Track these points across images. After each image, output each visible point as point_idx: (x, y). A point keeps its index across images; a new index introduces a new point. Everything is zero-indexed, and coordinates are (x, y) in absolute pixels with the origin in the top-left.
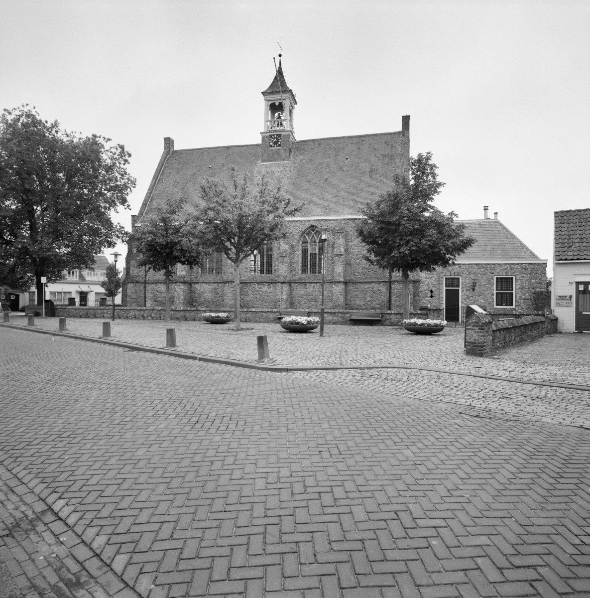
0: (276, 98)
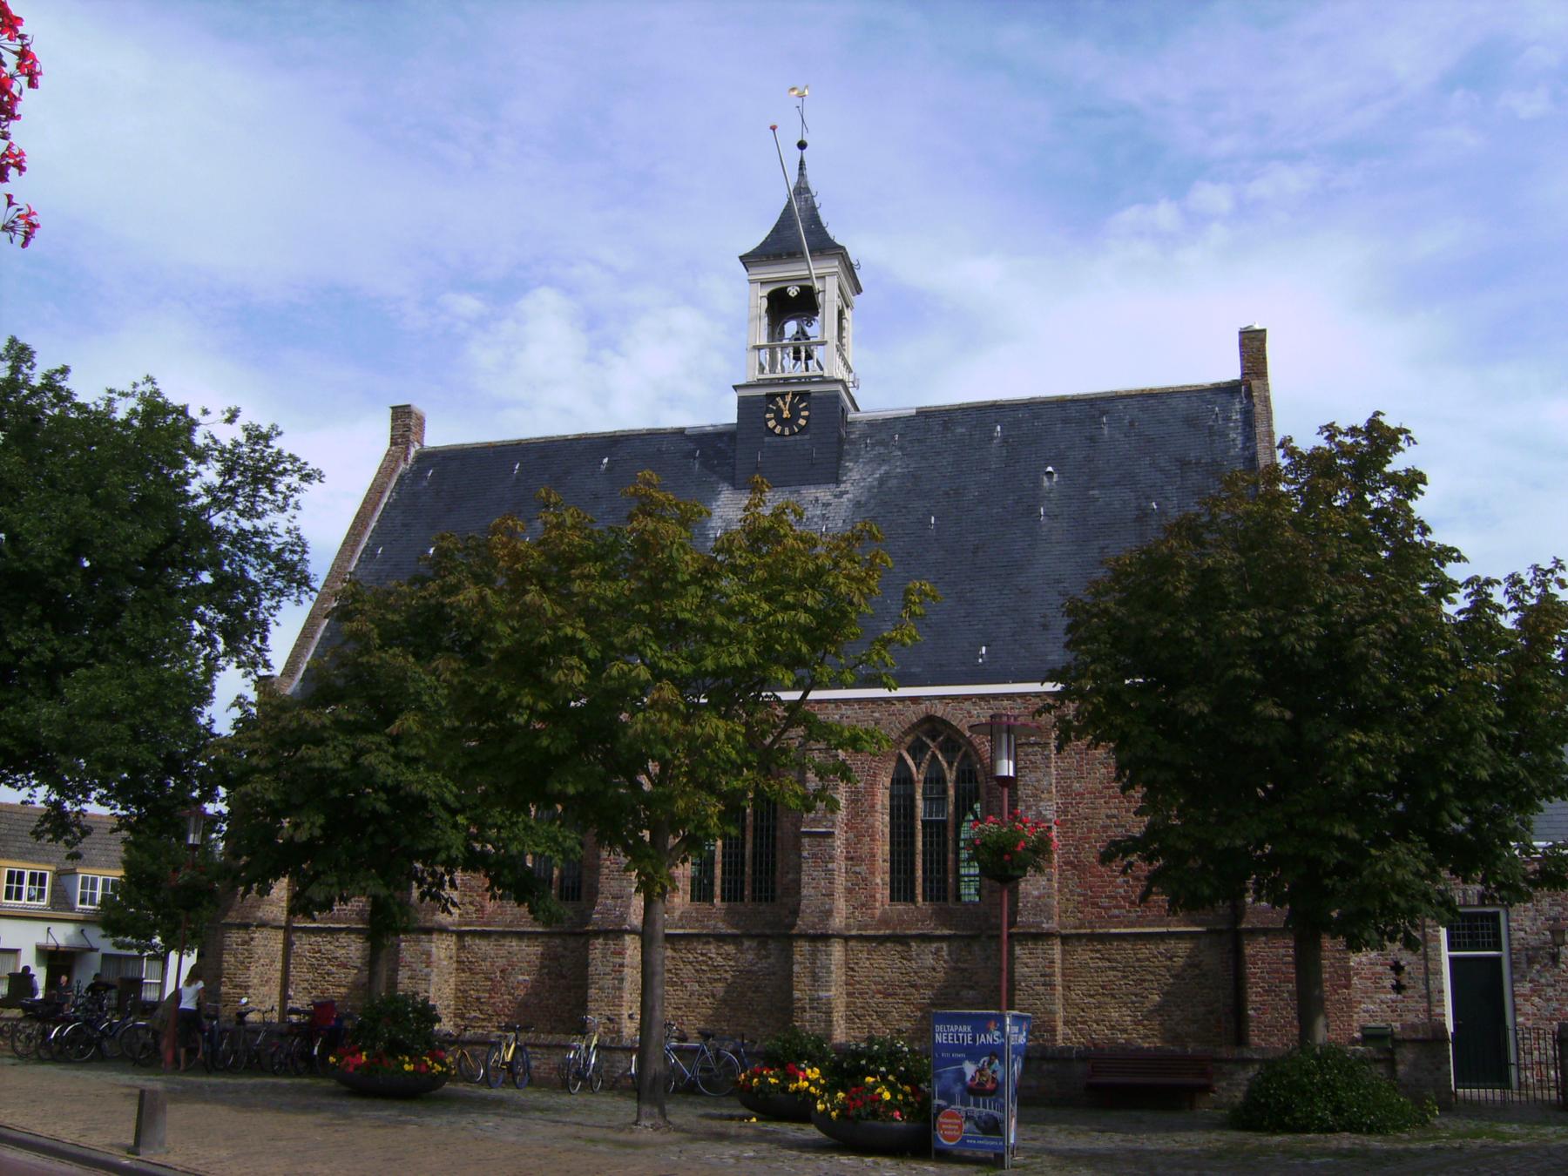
0: (786, 273)
